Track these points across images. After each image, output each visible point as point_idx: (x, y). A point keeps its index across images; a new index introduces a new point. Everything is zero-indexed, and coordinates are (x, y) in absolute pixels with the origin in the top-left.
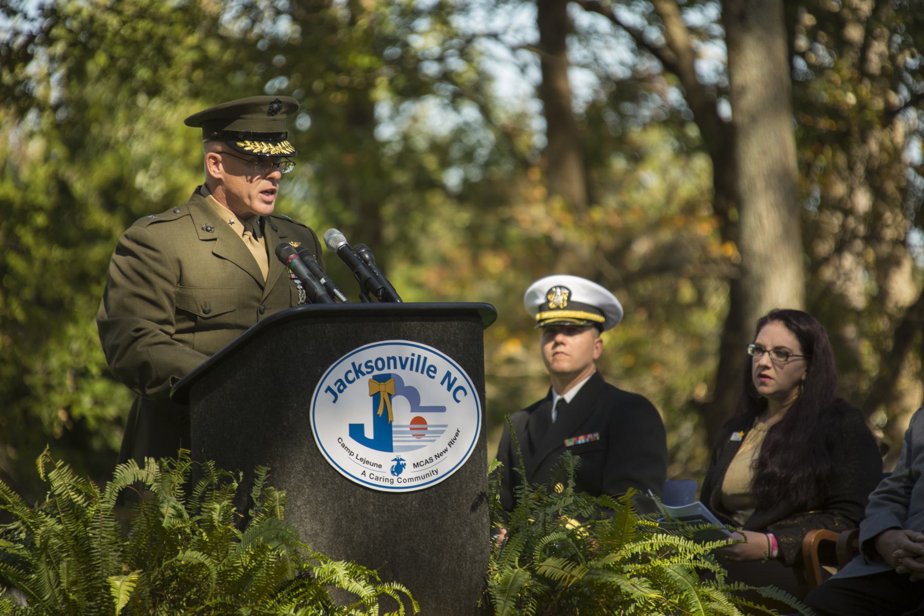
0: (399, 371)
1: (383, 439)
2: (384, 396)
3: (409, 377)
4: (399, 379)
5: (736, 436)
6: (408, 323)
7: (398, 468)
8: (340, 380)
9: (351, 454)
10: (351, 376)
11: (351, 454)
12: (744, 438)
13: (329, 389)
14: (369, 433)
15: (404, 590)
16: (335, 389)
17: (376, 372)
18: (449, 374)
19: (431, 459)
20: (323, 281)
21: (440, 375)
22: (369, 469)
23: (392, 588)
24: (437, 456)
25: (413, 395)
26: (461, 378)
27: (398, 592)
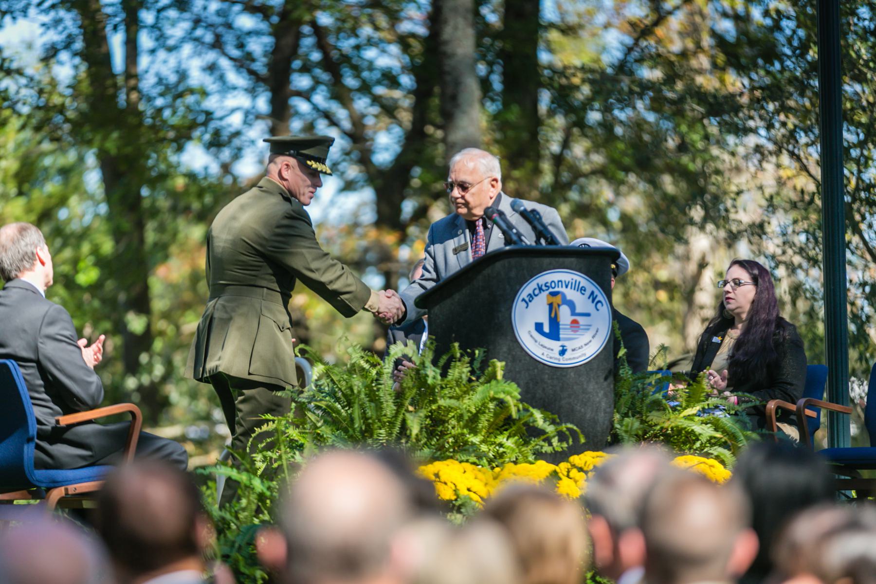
0: (563, 290)
1: (554, 334)
2: (555, 305)
4: (564, 296)
7: (563, 352)
8: (530, 295)
9: (536, 341)
10: (537, 292)
11: (536, 341)
12: (722, 341)
13: (523, 300)
14: (546, 329)
16: (527, 299)
17: (551, 290)
18: (592, 293)
21: (588, 293)
22: (546, 352)
25: (571, 305)
27: (568, 429)
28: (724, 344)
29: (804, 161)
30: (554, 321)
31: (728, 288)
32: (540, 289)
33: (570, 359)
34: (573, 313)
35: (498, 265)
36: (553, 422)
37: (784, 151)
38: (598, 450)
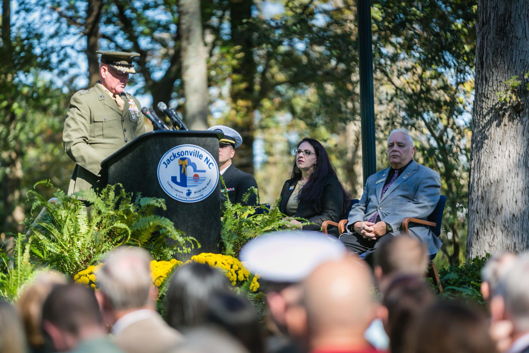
0: (189, 156)
1: (183, 182)
2: (184, 166)
3: (193, 159)
4: (189, 160)
5: (292, 188)
6: (187, 138)
7: (189, 194)
8: (168, 160)
9: (172, 187)
10: (172, 158)
11: (172, 187)
12: (294, 188)
13: (164, 163)
14: (178, 180)
15: (194, 239)
16: (166, 163)
17: (181, 157)
18: (207, 158)
19: (201, 190)
20: (160, 122)
21: (204, 158)
22: (179, 194)
23: (190, 238)
24: (203, 189)
25: (194, 166)
26: (212, 160)
27: (192, 240)
28: (295, 190)
29: (390, 76)
30: (183, 176)
31: (301, 154)
32: (175, 156)
33: (193, 198)
34: (195, 170)
35: (149, 142)
36: (183, 236)
37: (378, 70)
38: (208, 252)
